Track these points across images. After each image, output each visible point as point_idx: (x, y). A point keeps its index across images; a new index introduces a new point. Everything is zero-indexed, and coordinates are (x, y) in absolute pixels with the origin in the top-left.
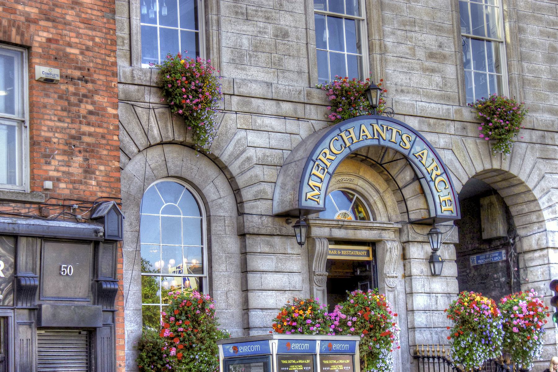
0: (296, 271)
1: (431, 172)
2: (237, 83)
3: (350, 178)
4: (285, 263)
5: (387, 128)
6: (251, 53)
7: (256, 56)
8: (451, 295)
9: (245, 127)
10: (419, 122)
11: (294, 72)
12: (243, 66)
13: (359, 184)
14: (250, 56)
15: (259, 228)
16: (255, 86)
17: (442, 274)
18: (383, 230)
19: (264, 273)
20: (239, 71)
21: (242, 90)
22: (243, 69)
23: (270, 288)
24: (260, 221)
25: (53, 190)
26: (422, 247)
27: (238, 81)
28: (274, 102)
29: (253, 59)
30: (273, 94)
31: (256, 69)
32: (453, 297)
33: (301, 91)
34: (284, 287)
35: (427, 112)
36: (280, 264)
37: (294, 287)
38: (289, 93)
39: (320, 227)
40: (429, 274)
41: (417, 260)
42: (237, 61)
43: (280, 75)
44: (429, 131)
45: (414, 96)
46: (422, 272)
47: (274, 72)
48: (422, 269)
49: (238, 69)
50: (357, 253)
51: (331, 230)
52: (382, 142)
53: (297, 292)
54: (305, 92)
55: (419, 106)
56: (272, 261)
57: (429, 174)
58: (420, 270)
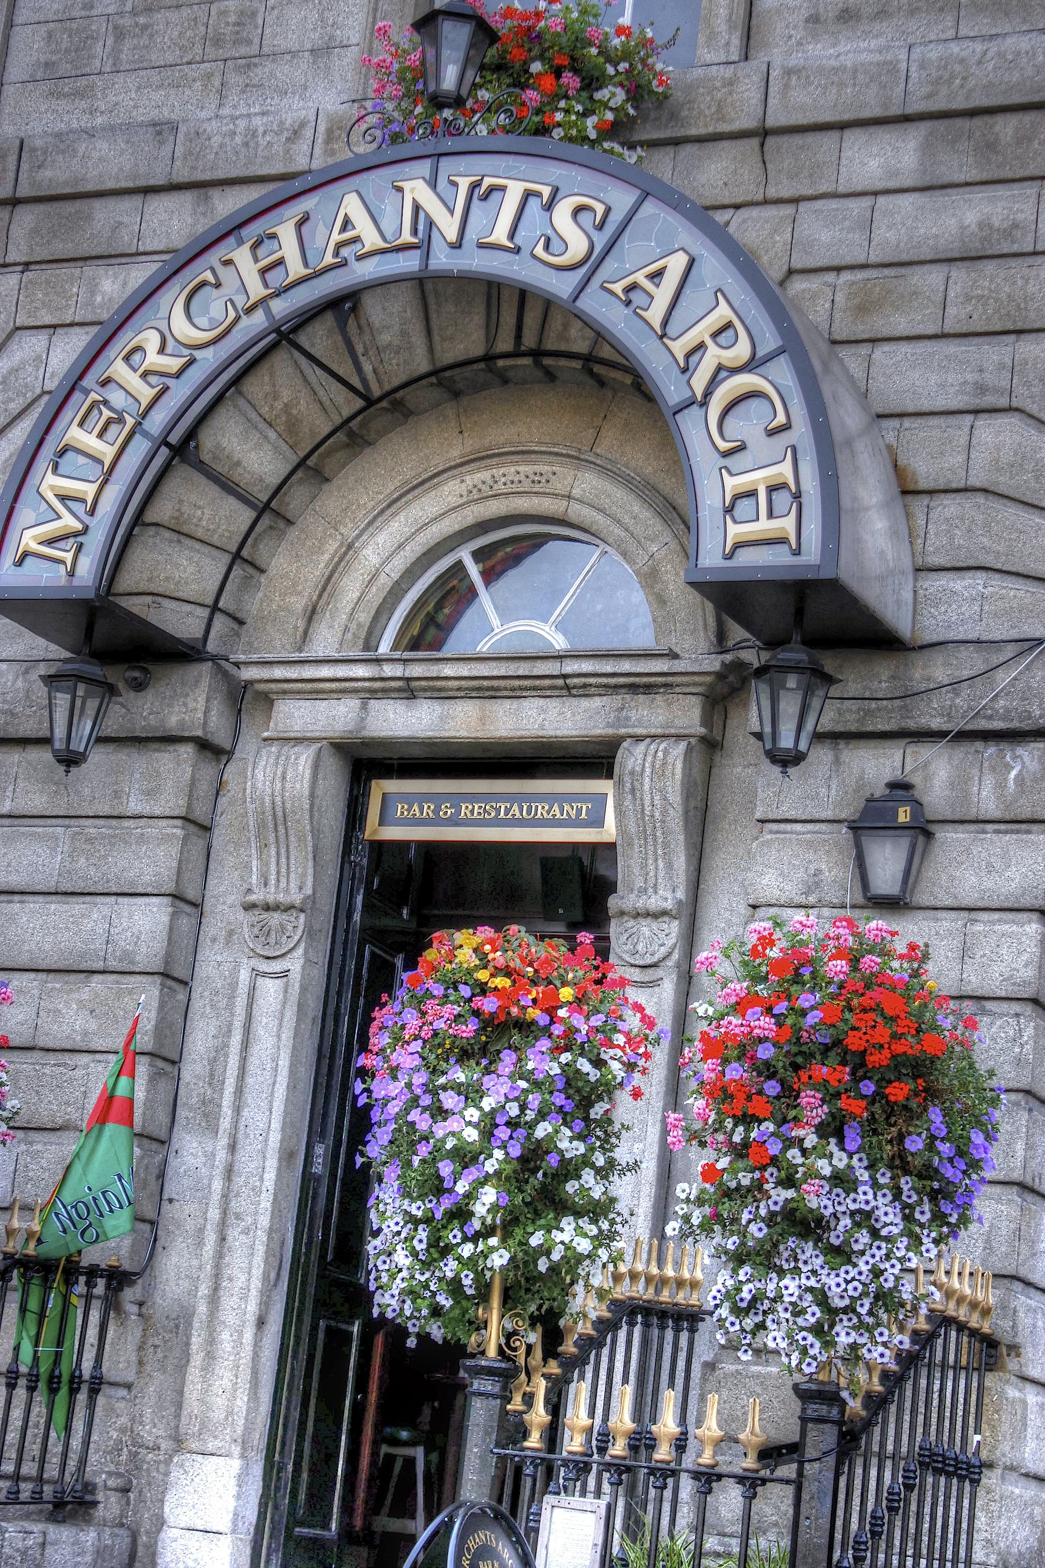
0: (149, 890)
1: (153, 379)
2: (33, 150)
3: (538, 468)
4: (105, 857)
5: (475, 186)
6: (127, 22)
7: (145, 27)
8: (989, 1005)
9: (48, 320)
10: (927, 149)
11: (294, 54)
12: (82, 82)
13: (576, 492)
14: (120, 35)
15: (12, 714)
16: (105, 146)
17: (922, 897)
18: (633, 688)
19: (17, 898)
20: (63, 104)
21: (48, 173)
22: (79, 94)
23: (23, 961)
24: (20, 684)
25: (784, 688)
26: (837, 761)
27: (39, 143)
28: (187, 198)
29: (128, 44)
30: (178, 163)
31: (131, 81)
32: (1002, 1015)
33: (303, 125)
34: (82, 956)
35: (971, 83)
36: (82, 860)
37: (126, 955)
38: (246, 144)
39: (317, 695)
40: (860, 899)
41: (798, 827)
42: (65, 68)
43: (233, 78)
44: (984, 176)
45: (913, 24)
46: (814, 884)
47: (209, 76)
48: (818, 872)
49: (60, 95)
50: (541, 810)
51: (364, 707)
52: (442, 259)
53: (139, 978)
54: (322, 128)
55: (922, 66)
56: (54, 849)
57: (165, 389)
58: (801, 874)
